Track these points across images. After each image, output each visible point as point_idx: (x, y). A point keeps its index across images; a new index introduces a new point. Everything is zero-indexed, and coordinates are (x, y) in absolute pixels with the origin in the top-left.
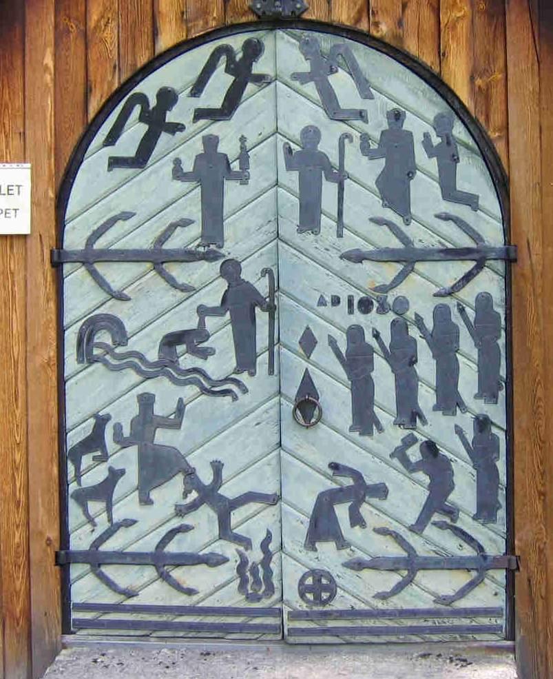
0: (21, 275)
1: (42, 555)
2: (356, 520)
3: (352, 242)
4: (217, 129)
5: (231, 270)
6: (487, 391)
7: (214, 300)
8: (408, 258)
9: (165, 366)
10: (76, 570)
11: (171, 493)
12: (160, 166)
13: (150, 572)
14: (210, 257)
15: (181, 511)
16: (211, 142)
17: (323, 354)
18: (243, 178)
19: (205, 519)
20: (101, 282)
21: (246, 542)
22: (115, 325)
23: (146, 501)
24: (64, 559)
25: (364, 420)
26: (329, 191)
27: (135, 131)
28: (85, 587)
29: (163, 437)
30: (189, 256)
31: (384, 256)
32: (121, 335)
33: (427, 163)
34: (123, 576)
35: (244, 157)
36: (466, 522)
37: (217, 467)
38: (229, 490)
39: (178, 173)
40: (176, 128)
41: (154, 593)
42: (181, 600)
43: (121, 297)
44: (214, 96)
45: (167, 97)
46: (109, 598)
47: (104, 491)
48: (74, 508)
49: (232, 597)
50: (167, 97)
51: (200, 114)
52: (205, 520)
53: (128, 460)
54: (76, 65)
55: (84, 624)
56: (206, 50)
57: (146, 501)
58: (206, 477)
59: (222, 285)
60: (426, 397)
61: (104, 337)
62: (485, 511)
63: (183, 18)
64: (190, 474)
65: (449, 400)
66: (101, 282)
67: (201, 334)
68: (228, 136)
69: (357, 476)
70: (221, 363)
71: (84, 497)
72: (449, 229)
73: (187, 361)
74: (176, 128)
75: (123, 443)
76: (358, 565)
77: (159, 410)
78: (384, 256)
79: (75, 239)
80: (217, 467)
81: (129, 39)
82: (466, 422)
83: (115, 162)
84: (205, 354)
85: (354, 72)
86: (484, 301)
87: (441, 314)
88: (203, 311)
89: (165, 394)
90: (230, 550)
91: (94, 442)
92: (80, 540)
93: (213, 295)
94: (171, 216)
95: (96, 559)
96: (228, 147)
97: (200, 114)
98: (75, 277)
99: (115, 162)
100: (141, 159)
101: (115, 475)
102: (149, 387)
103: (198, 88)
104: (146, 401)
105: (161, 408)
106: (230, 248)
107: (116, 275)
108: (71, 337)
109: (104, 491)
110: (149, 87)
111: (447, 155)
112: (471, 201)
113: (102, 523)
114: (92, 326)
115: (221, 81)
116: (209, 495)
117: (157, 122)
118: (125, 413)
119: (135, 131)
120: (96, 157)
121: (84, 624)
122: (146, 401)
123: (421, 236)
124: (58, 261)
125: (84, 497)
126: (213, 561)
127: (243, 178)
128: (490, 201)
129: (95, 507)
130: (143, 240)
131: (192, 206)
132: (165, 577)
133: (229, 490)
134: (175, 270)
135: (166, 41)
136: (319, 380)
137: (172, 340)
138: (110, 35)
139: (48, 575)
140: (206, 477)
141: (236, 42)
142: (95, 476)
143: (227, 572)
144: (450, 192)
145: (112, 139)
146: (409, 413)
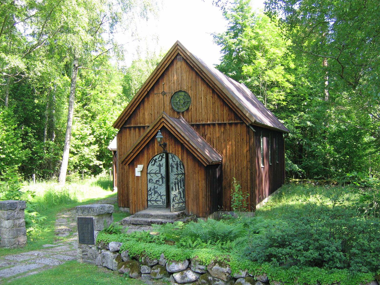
0: (126, 160)
1: (146, 200)
2: (176, 199)
3: (175, 173)
4: (160, 162)
5: (161, 175)
6: (183, 186)
7: (160, 177)
8: (178, 174)
9: (156, 183)
10: (148, 202)
11: (156, 195)
12: (156, 165)
13: (155, 202)
14: (160, 173)
15: (157, 196)
16: (160, 163)
17: (173, 184)
18: (162, 166)
19: (159, 197)
20: (151, 176)
21: (163, 199)
22: (152, 180)
23: (154, 195)
24: (147, 201)
25: (176, 190)
26: (173, 168)
27: (153, 162)
28: (149, 203)
29: (156, 190)
30: (158, 173)
31: (177, 174)
32: (152, 180)
33: (179, 166)
34: (153, 202)
35: (162, 165)
36: (182, 199)
37: (160, 192)
38: (161, 195)
39: (157, 166)
40: (157, 162)
41: (155, 204)
42: (157, 205)
43: (152, 177)
44: (160, 159)
45: (156, 159)
46: (151, 204)
47: (151, 194)
48: (148, 196)
49: (162, 204)
50: (156, 159)
51: (159, 161)
52: (159, 197)
53: (153, 192)
54: (148, 156)
55: (149, 207)
56: (159, 155)
57: (154, 195)
58: (159, 193)
59: (161, 176)
60: (180, 187)
61: (151, 181)
62: (183, 197)
63: (157, 152)
64: (158, 193)
65: (181, 187)
66: (151, 176)
67: (159, 180)
68: (161, 163)
69: (176, 195)
70: (161, 183)
71: (149, 195)
72: (181, 172)
73: (158, 183)
74: (157, 162)
75: (153, 190)
76: (176, 204)
77: (156, 187)
78: (177, 174)
79: (148, 172)
80: (160, 192)
81: (153, 154)
82: (182, 189)
83: (152, 165)
84: (159, 182)
85: (174, 158)
86: (183, 178)
87: (180, 179)
88: (159, 178)
89: (156, 186)
90: (161, 200)
91: (150, 190)
92: (149, 199)
93: (160, 177)
94: (156, 170)
95: (150, 201)
96: (161, 164)
97: (159, 161)
98: (148, 175)
99: (152, 165)
100: (154, 165)
101: (152, 193)
102: (155, 185)
103: (158, 159)
104: (154, 186)
105: (156, 187)
106: (161, 173)
107: (152, 175)
108: (148, 181)
109: (151, 194)
110: (155, 158)
111: (180, 165)
112: (182, 169)
113: (151, 197)
114: (150, 179)
115: (161, 158)
116: (160, 195)
117: (155, 161)
118: (153, 187)
119: (153, 162)
120: (150, 164)
121: (149, 207)
122: (154, 186)
123: (179, 173)
124: (147, 173)
125: (149, 195)
126: (160, 201)
127: (162, 166)
128: (183, 169)
129: (150, 196)
130: (154, 172)
131: (158, 169)
132: (156, 202)
133: (161, 195)
134: (157, 175)
135: (156, 154)
136: (173, 186)
137: (157, 181)
138: (151, 154)
139: (146, 202)
140: (159, 193)
141: (162, 154)
142: (150, 193)
143: (161, 202)
144: (181, 168)
145: (151, 163)
146: (179, 189)
